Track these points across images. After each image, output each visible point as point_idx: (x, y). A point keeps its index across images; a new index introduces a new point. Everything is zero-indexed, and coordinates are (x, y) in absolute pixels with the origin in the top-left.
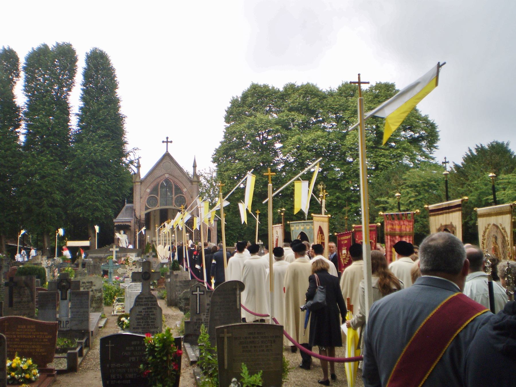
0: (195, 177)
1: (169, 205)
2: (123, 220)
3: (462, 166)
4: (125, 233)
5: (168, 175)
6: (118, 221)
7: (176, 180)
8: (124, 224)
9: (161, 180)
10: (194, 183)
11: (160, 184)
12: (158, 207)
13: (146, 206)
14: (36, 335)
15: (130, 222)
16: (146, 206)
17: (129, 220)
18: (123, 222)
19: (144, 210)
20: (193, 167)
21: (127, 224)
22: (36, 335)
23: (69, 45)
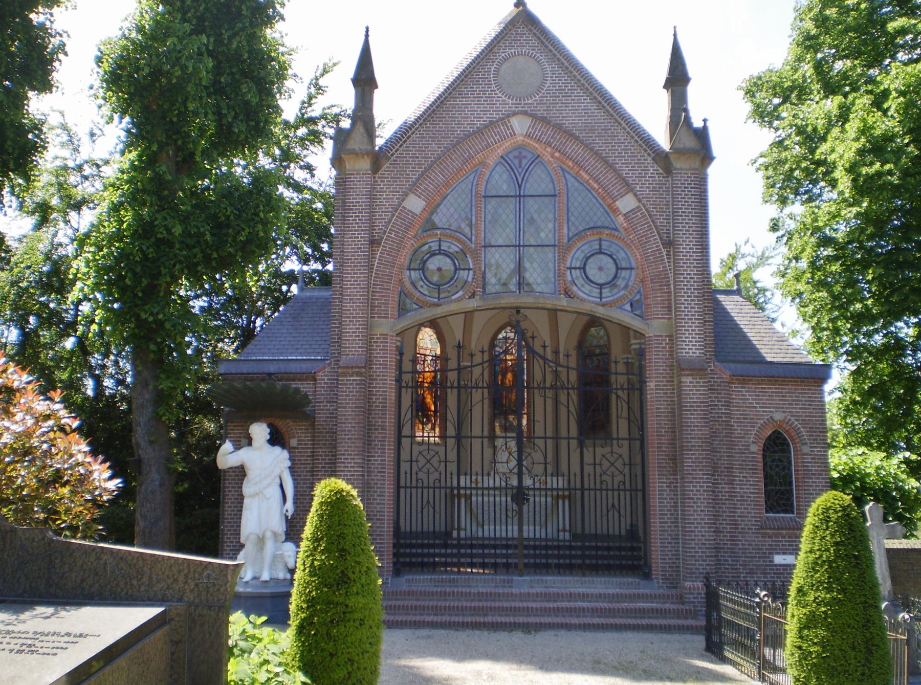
5: (527, 121)
15: (311, 377)
17: (304, 367)
19: (393, 309)
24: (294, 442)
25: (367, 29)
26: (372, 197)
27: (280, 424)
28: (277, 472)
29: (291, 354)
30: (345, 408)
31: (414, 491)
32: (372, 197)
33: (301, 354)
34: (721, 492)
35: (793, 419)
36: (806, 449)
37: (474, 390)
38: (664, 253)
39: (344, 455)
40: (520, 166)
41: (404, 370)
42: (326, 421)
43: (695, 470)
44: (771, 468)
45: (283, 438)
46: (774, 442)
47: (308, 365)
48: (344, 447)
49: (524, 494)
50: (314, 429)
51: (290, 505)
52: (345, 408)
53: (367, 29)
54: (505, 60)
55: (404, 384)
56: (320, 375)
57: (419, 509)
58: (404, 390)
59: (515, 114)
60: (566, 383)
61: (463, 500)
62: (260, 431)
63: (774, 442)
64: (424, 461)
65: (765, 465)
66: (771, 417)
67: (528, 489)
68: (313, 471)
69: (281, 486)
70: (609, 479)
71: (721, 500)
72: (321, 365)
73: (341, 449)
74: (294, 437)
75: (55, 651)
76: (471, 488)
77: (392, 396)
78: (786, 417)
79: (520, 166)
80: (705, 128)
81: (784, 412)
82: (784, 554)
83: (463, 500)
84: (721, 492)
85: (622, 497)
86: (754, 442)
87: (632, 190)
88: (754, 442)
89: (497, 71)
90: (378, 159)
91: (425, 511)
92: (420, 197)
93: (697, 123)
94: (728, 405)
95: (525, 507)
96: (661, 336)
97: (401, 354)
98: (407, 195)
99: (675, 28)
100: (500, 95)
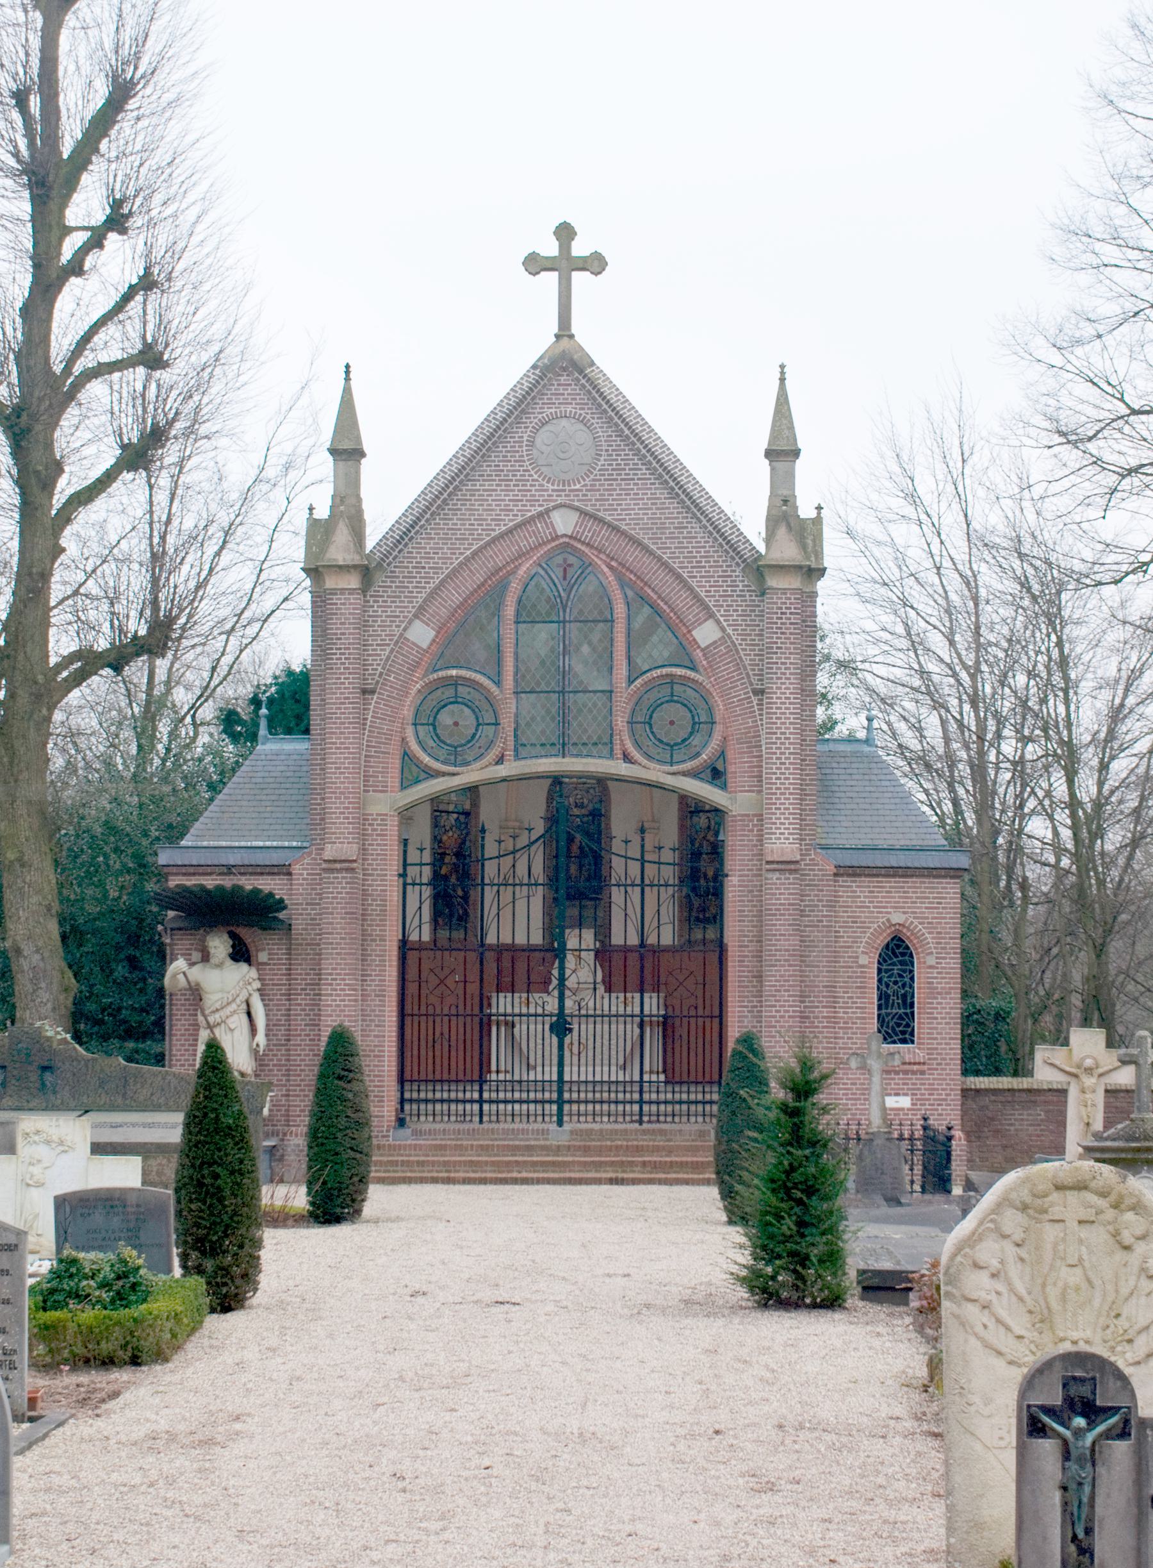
0: (782, 531)
1: (587, 747)
2: (232, 859)
3: (367, 552)
4: (241, 953)
5: (574, 517)
6: (194, 858)
7: (631, 555)
8: (228, 882)
9: (522, 555)
10: (773, 582)
11: (515, 586)
12: (500, 760)
13: (407, 756)
14: (1037, 653)
15: (284, 870)
16: (407, 756)
17: (275, 858)
18: (229, 870)
19: (393, 778)
20: (769, 454)
21: (248, 883)
22: (1037, 653)
23: (576, 234)
24: (263, 957)
25: (348, 367)
26: (364, 625)
27: (242, 932)
28: (243, 996)
29: (257, 838)
30: (332, 913)
31: (423, 1018)
32: (364, 625)
33: (269, 838)
34: (817, 1017)
35: (916, 922)
36: (931, 961)
37: (502, 888)
38: (755, 703)
39: (331, 974)
40: (565, 578)
41: (409, 861)
42: (306, 929)
43: (779, 991)
44: (887, 986)
45: (248, 951)
46: (893, 951)
47: (281, 853)
48: (331, 964)
49: (566, 1022)
50: (290, 939)
51: (261, 1038)
52: (332, 913)
53: (348, 367)
54: (544, 424)
55: (409, 880)
56: (296, 869)
57: (430, 1044)
58: (409, 888)
59: (555, 508)
60: (623, 879)
61: (503, 1029)
62: (219, 945)
63: (893, 951)
64: (449, 982)
65: (880, 981)
66: (888, 920)
67: (572, 1016)
68: (290, 995)
69: (249, 1014)
70: (677, 1003)
71: (817, 1027)
72: (299, 854)
73: (327, 965)
74: (264, 950)
75: (676, 1037)
76: (514, 1015)
77: (395, 896)
78: (907, 919)
79: (565, 578)
80: (818, 521)
81: (904, 913)
82: (897, 1094)
83: (503, 1029)
84: (817, 1017)
85: (423, 1025)
86: (863, 952)
87: (711, 615)
88: (863, 952)
89: (531, 443)
90: (367, 572)
91: (437, 1046)
92: (428, 625)
93: (806, 511)
94: (832, 905)
95: (567, 1040)
96: (748, 815)
97: (405, 845)
98: (410, 622)
99: (782, 367)
100: (536, 477)
